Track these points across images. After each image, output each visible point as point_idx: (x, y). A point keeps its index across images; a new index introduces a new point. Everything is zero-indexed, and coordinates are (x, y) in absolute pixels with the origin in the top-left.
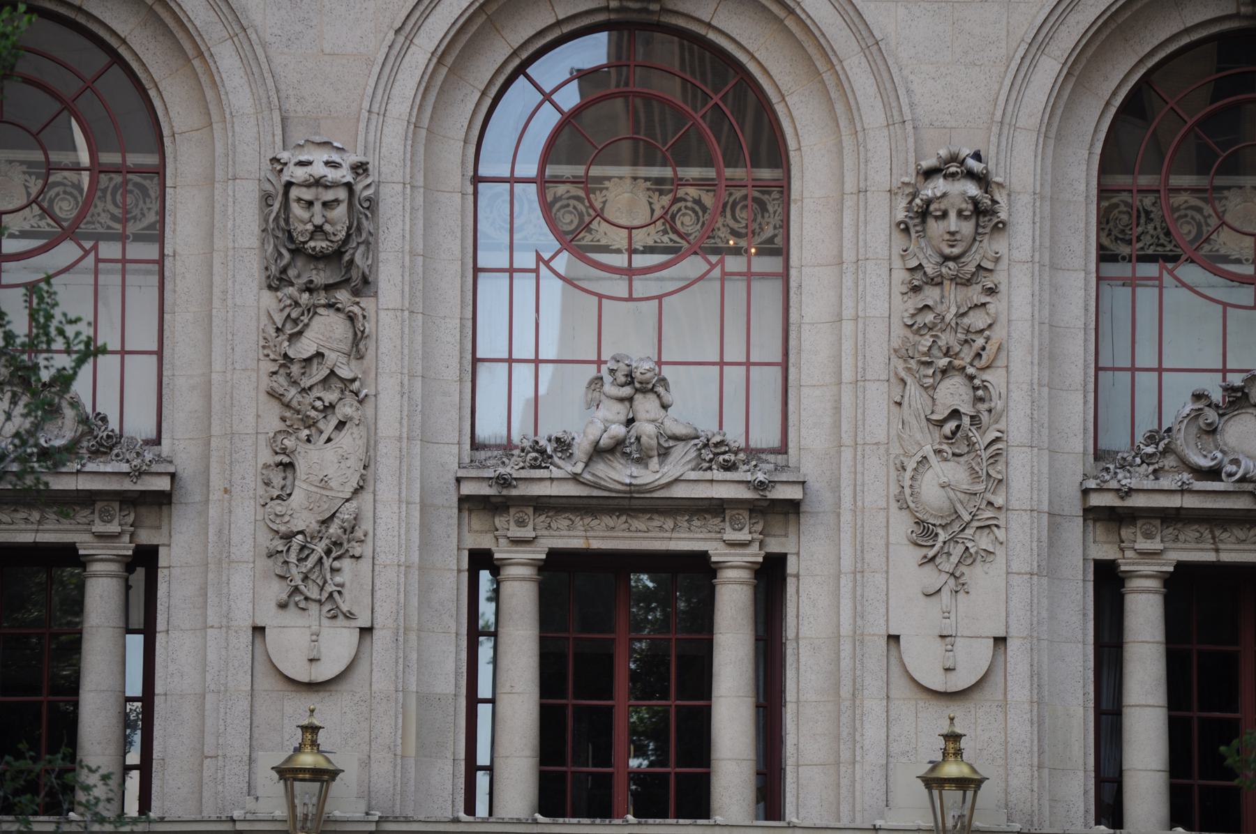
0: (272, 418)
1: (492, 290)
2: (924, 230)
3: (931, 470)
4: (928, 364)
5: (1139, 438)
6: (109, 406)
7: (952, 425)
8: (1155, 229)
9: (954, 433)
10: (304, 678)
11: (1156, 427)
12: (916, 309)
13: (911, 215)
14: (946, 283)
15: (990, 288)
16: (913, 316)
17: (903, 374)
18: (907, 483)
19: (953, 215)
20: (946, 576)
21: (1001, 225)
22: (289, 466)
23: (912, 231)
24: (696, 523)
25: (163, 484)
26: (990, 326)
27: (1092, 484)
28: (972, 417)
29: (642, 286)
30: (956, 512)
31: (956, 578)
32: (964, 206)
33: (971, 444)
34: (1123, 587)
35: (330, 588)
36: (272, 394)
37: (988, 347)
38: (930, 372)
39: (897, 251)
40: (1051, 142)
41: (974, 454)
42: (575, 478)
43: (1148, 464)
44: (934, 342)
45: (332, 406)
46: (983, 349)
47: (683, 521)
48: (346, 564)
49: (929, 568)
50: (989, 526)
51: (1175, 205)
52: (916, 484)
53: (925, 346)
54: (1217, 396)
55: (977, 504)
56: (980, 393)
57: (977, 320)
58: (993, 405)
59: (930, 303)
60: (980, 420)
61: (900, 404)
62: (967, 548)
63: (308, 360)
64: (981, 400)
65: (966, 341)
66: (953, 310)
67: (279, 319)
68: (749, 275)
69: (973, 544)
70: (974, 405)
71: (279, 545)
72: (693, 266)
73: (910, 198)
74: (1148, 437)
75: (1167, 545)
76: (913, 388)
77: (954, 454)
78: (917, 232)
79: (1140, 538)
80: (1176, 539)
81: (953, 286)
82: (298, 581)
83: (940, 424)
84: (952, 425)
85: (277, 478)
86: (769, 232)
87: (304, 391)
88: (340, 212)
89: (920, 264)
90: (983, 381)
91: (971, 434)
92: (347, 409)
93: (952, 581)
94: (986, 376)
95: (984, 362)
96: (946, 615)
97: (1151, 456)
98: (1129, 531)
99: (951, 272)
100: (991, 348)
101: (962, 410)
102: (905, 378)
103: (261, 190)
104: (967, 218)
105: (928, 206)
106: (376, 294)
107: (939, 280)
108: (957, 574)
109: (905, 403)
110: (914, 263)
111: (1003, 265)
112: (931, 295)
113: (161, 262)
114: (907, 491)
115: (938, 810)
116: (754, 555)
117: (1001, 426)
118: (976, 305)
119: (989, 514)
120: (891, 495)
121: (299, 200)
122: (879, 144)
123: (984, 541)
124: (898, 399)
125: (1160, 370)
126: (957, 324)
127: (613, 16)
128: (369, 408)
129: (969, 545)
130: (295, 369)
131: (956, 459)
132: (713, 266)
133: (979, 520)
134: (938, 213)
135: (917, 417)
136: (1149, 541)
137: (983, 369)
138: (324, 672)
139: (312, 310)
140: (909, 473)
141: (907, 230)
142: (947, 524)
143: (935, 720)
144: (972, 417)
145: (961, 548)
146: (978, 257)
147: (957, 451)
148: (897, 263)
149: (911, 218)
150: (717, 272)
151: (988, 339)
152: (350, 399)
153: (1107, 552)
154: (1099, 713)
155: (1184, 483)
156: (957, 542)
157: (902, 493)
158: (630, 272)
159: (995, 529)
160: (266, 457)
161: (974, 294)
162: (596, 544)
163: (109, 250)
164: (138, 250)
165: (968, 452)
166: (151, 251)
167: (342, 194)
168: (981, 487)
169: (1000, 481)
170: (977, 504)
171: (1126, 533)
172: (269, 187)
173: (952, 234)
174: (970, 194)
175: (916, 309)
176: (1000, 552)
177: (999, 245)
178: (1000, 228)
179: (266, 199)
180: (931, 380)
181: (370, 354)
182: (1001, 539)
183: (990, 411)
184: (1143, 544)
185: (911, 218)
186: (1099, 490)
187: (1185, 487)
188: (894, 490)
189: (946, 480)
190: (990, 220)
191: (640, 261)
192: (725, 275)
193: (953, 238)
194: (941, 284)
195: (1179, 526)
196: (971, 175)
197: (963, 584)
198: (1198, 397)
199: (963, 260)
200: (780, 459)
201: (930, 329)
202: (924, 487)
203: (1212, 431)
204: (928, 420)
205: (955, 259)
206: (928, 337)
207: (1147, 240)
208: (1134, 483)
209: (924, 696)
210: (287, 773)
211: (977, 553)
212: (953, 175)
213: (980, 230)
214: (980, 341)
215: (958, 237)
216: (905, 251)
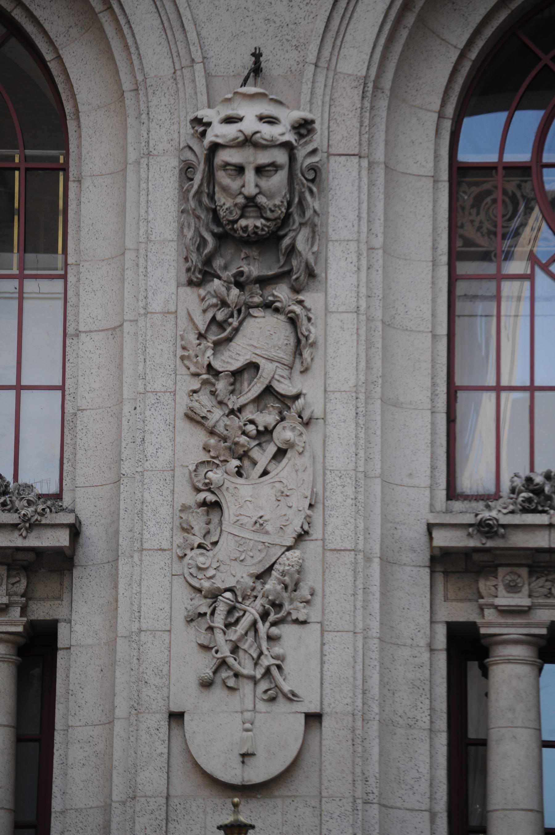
34: (487, 656)
35: (266, 661)
63: (237, 374)
82: (225, 651)
98: (488, 583)
171: (484, 585)
172: (189, 155)
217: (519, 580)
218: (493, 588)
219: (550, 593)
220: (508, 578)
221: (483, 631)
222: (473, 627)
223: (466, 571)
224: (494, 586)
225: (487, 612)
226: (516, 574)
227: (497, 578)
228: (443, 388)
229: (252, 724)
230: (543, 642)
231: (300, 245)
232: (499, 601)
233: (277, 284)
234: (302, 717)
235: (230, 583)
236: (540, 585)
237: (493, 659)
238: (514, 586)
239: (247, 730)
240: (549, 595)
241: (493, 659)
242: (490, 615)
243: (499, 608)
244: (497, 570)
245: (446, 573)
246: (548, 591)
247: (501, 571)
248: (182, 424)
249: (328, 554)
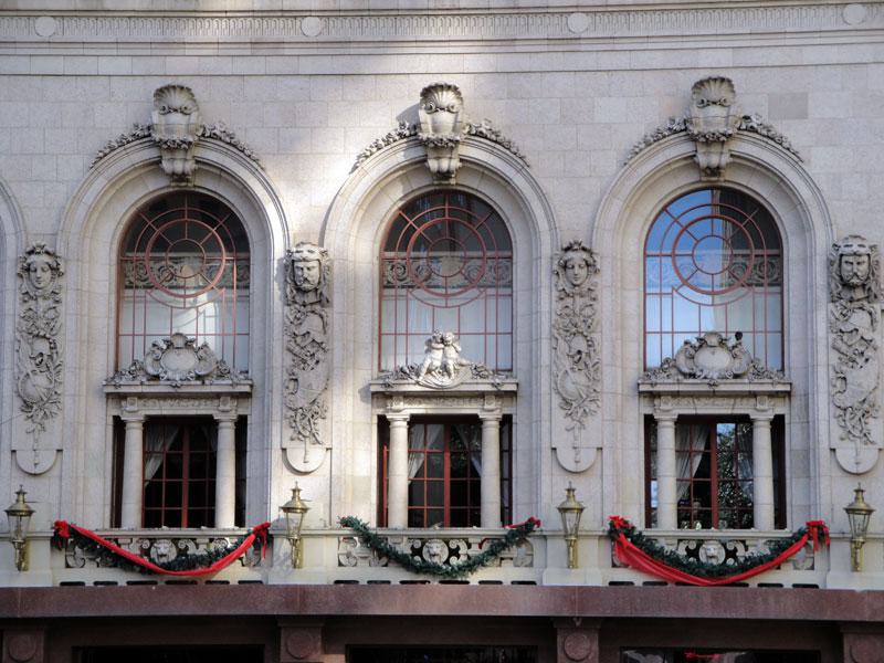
0: (288, 360)
1: (653, 302)
6: (761, 355)
10: (855, 471)
19: (577, 267)
22: (296, 380)
24: (209, 402)
25: (247, 389)
29: (452, 302)
33: (586, 365)
35: (864, 431)
36: (289, 350)
42: (418, 383)
45: (862, 353)
47: (203, 402)
48: (871, 420)
49: (569, 419)
54: (695, 342)
57: (588, 311)
63: (304, 335)
64: (590, 346)
67: (291, 318)
68: (497, 296)
71: (842, 413)
72: (473, 292)
82: (850, 428)
83: (34, 359)
84: (40, 359)
85: (292, 385)
86: (776, 276)
87: (850, 346)
88: (864, 267)
92: (319, 355)
93: (39, 427)
95: (54, 332)
100: (58, 325)
103: (828, 259)
106: (332, 307)
112: (569, 301)
113: (511, 295)
115: (852, 523)
116: (498, 414)
121: (846, 262)
122: (546, 238)
123: (593, 406)
125: (145, 335)
127: (437, 188)
128: (329, 355)
130: (299, 340)
132: (481, 292)
138: (581, 467)
139: (305, 314)
141: (21, 276)
143: (853, 484)
148: (554, 289)
150: (483, 295)
152: (321, 351)
153: (380, 411)
154: (502, 480)
158: (446, 296)
160: (286, 377)
161: (587, 300)
162: (165, 413)
163: (491, 291)
164: (502, 291)
166: (508, 291)
167: (866, 258)
171: (123, 403)
172: (832, 258)
177: (595, 279)
178: (61, 275)
179: (831, 263)
181: (329, 332)
184: (663, 407)
188: (15, 389)
191: (450, 291)
192: (486, 296)
194: (36, 299)
196: (584, 249)
198: (686, 343)
200: (509, 374)
203: (692, 357)
207: (408, 279)
209: (845, 474)
210: (850, 511)
212: (39, 253)
228: (377, 333)
231: (873, 288)
235: (850, 405)
248: (286, 352)
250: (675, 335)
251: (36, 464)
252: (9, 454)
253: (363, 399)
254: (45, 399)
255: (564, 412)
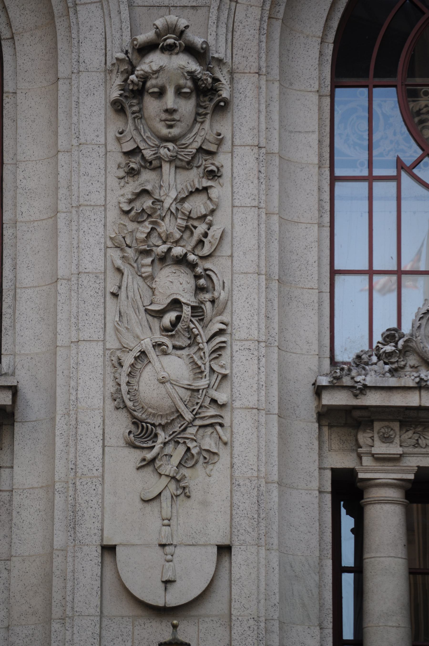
2: (140, 110)
3: (149, 367)
4: (147, 253)
5: (377, 338)
7: (172, 316)
8: (395, 134)
9: (174, 324)
11: (395, 326)
12: (133, 194)
13: (127, 94)
14: (166, 167)
15: (212, 171)
16: (130, 201)
17: (119, 263)
18: (124, 379)
20: (167, 480)
21: (222, 104)
23: (129, 112)
26: (213, 212)
27: (324, 381)
28: (193, 308)
30: (178, 411)
31: (178, 481)
32: (182, 82)
34: (362, 498)
37: (210, 233)
38: (148, 260)
39: (112, 132)
40: (278, 24)
41: (197, 348)
43: (386, 363)
44: (152, 229)
46: (206, 235)
49: (149, 470)
50: (211, 425)
51: (415, 110)
52: (133, 381)
53: (143, 232)
55: (200, 401)
56: (202, 282)
58: (216, 294)
59: (149, 187)
60: (203, 311)
61: (115, 295)
62: (188, 449)
65: (187, 227)
66: (173, 194)
69: (195, 444)
70: (196, 294)
73: (125, 76)
74: (388, 336)
75: (406, 450)
76: (130, 277)
77: (175, 347)
78: (133, 113)
79: (377, 442)
80: (417, 445)
81: (173, 169)
84: (172, 316)
89: (138, 147)
90: (206, 270)
91: (192, 326)
93: (173, 486)
94: (208, 265)
96: (166, 522)
97: (390, 355)
98: (366, 435)
99: (169, 153)
101: (183, 300)
102: (122, 267)
104: (186, 96)
105: (144, 83)
107: (155, 163)
108: (178, 477)
109: (123, 295)
110: (129, 147)
111: (226, 146)
114: (124, 388)
117: (225, 318)
118: (197, 190)
119: (212, 412)
120: (108, 394)
124: (114, 289)
126: (177, 209)
129: (191, 445)
131: (179, 352)
133: (202, 418)
134: (156, 90)
135: (136, 310)
136: (385, 445)
137: (203, 258)
140: (126, 369)
142: (167, 424)
144: (193, 308)
145: (181, 449)
146: (199, 140)
147: (178, 343)
148: (113, 146)
149: (126, 97)
151: (210, 225)
155: (422, 379)
156: (178, 443)
157: (119, 391)
159: (218, 428)
165: (189, 346)
168: (202, 383)
169: (225, 376)
170: (200, 401)
173: (170, 111)
174: (189, 69)
175: (133, 194)
176: (224, 452)
180: (149, 269)
182: (225, 438)
183: (213, 302)
185: (126, 97)
186: (331, 387)
187: (423, 384)
188: (111, 388)
189: (165, 375)
190: (211, 100)
193: (169, 117)
195: (419, 429)
197: (184, 488)
199: (183, 142)
201: (149, 216)
202: (142, 384)
204: (146, 310)
205: (173, 140)
206: (146, 223)
208: (370, 380)
211: (199, 453)
213: (201, 111)
214: (202, 228)
215: (176, 116)
216: (121, 133)
217: (392, 433)
218: (370, 440)
219: (418, 444)
220: (383, 430)
221: (361, 476)
222: (352, 472)
223: (346, 425)
224: (370, 438)
225: (364, 459)
226: (388, 427)
227: (373, 431)
229: (172, 556)
230: (409, 486)
232: (375, 450)
233: (194, 61)
234: (215, 550)
236: (410, 436)
237: (366, 500)
238: (388, 438)
239: (168, 561)
240: (416, 445)
241: (366, 500)
242: (367, 461)
243: (375, 456)
244: (373, 424)
245: (330, 426)
246: (416, 441)
247: (377, 425)
249: (415, 171)
250: (366, 278)
251: (167, 583)
252: (96, 552)
253: (114, 407)
254: (188, 416)
255: (137, 455)
